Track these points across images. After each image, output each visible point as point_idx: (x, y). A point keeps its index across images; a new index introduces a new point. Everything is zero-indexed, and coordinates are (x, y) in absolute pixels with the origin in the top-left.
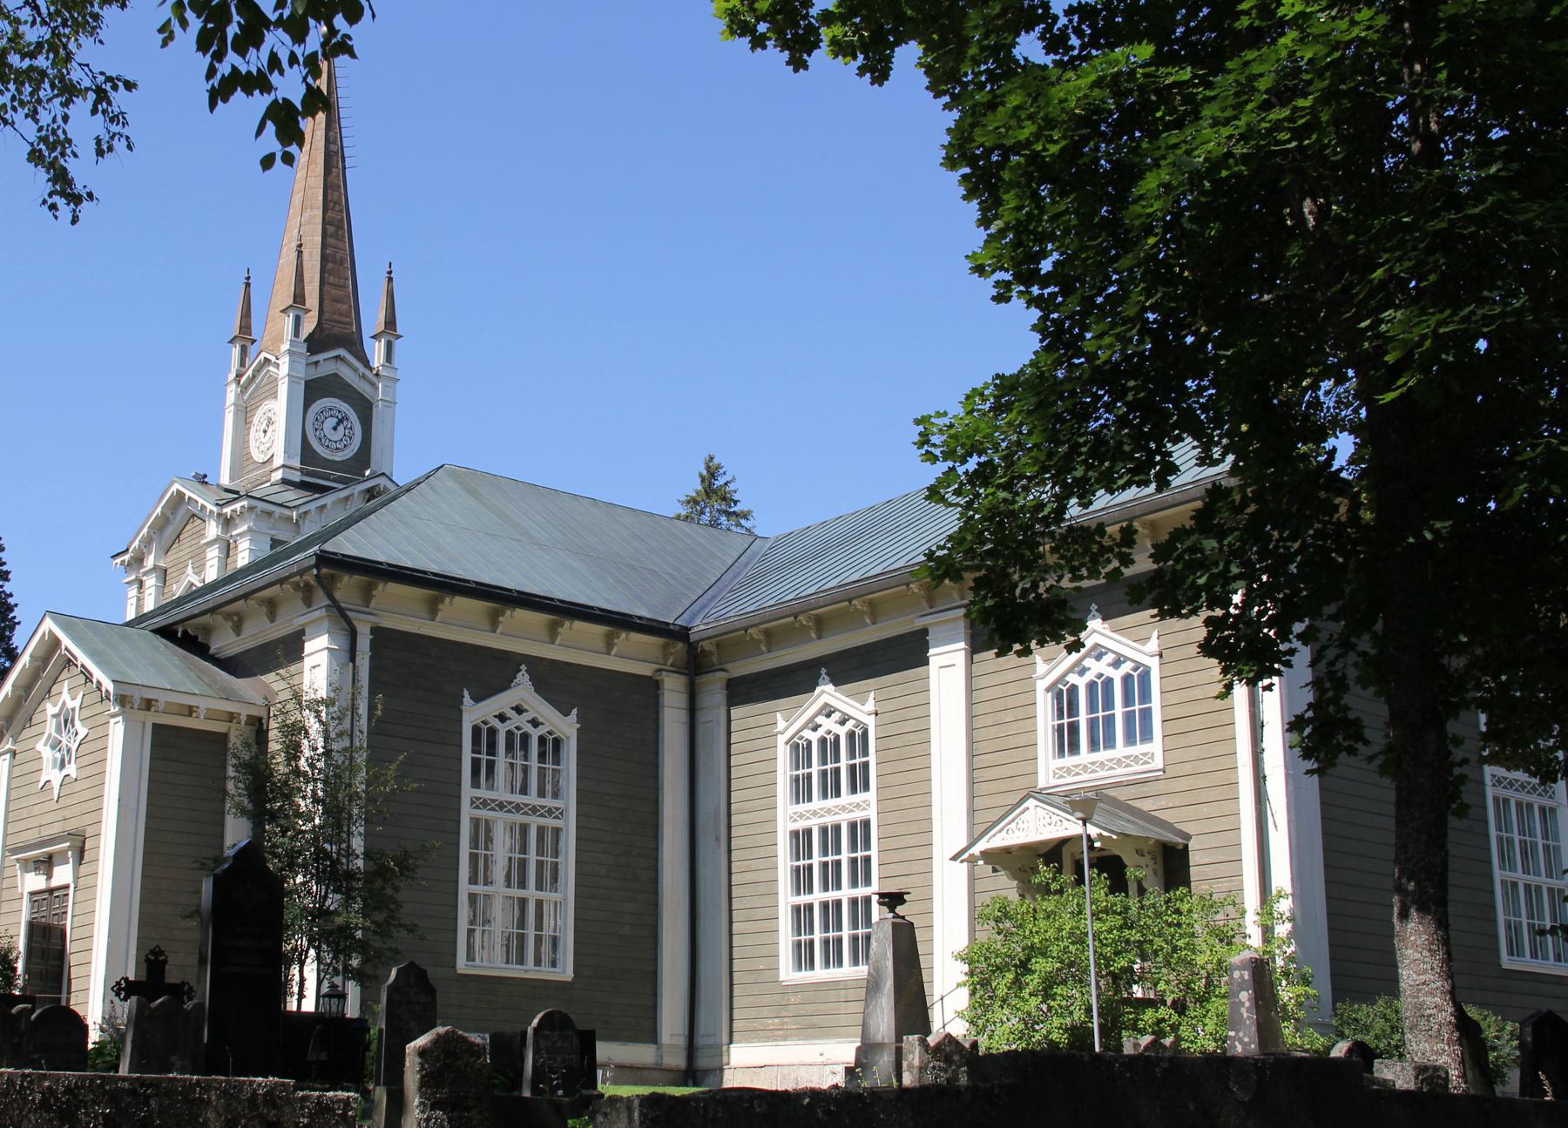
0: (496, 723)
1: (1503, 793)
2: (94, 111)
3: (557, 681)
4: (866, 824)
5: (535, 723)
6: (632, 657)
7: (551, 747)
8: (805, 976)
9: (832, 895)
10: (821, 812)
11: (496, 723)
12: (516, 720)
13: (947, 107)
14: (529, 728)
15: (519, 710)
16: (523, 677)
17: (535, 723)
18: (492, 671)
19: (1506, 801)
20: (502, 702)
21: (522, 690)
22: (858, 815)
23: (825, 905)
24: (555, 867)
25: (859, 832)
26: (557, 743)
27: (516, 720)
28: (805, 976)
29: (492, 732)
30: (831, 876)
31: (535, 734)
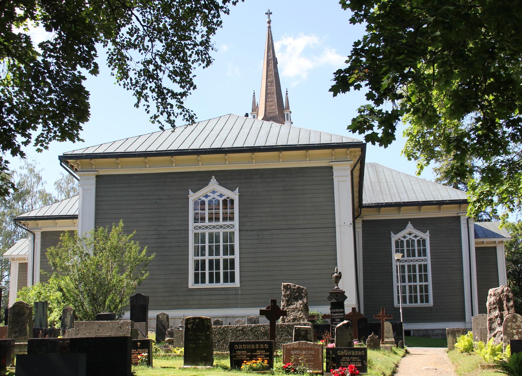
3: (226, 178)
4: (426, 266)
5: (221, 196)
7: (228, 203)
8: (200, 286)
10: (208, 228)
11: (403, 239)
13: (353, 21)
15: (214, 192)
17: (416, 237)
21: (410, 228)
27: (411, 237)
28: (200, 286)
30: (413, 278)
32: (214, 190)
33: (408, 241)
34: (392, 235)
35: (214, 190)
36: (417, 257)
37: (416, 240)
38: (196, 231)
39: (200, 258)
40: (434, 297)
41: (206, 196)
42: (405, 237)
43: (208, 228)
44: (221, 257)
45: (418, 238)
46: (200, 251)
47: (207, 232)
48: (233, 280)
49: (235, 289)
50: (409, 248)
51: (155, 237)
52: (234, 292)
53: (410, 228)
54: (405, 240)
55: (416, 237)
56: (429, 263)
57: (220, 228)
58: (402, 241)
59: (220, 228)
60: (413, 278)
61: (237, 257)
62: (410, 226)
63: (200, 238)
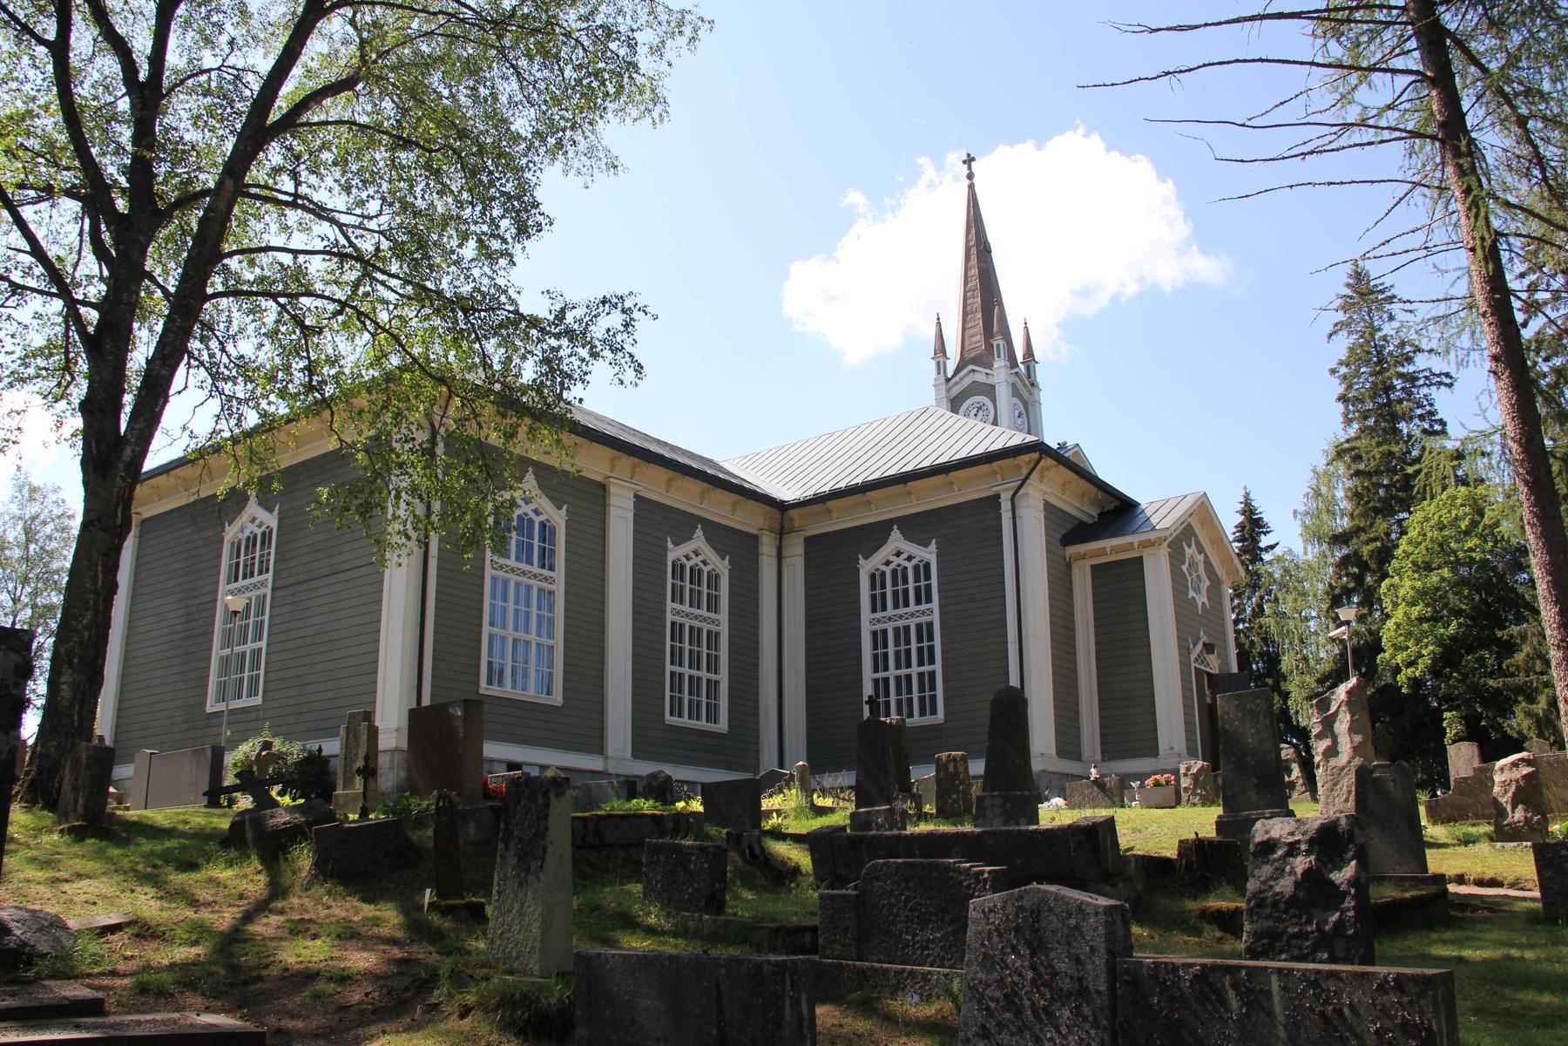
0: (884, 568)
1: (679, 619)
2: (566, 173)
3: (916, 527)
4: (930, 625)
6: (746, 519)
7: (923, 570)
9: (903, 672)
10: (893, 618)
11: (884, 568)
12: (901, 560)
13: (1348, 285)
14: (906, 563)
16: (699, 533)
18: (874, 536)
19: (682, 626)
20: (885, 552)
21: (896, 540)
22: (923, 619)
23: (898, 678)
24: (875, 648)
25: (925, 631)
26: (717, 577)
27: (901, 560)
29: (700, 571)
30: (904, 659)
31: (706, 569)
32: (898, 549)
33: (894, 572)
34: (862, 561)
35: (898, 549)
36: (913, 608)
37: (910, 565)
38: (874, 628)
39: (881, 675)
40: (945, 698)
41: (888, 563)
42: (888, 563)
43: (893, 618)
44: (915, 669)
45: (914, 561)
46: (880, 663)
47: (890, 627)
48: (934, 712)
49: (937, 727)
50: (899, 588)
51: (181, 612)
52: (253, 716)
53: (896, 540)
54: (888, 570)
55: (909, 559)
56: (936, 618)
57: (913, 615)
58: (883, 574)
59: (913, 615)
60: (904, 659)
61: (938, 667)
62: (896, 534)
63: (879, 638)
